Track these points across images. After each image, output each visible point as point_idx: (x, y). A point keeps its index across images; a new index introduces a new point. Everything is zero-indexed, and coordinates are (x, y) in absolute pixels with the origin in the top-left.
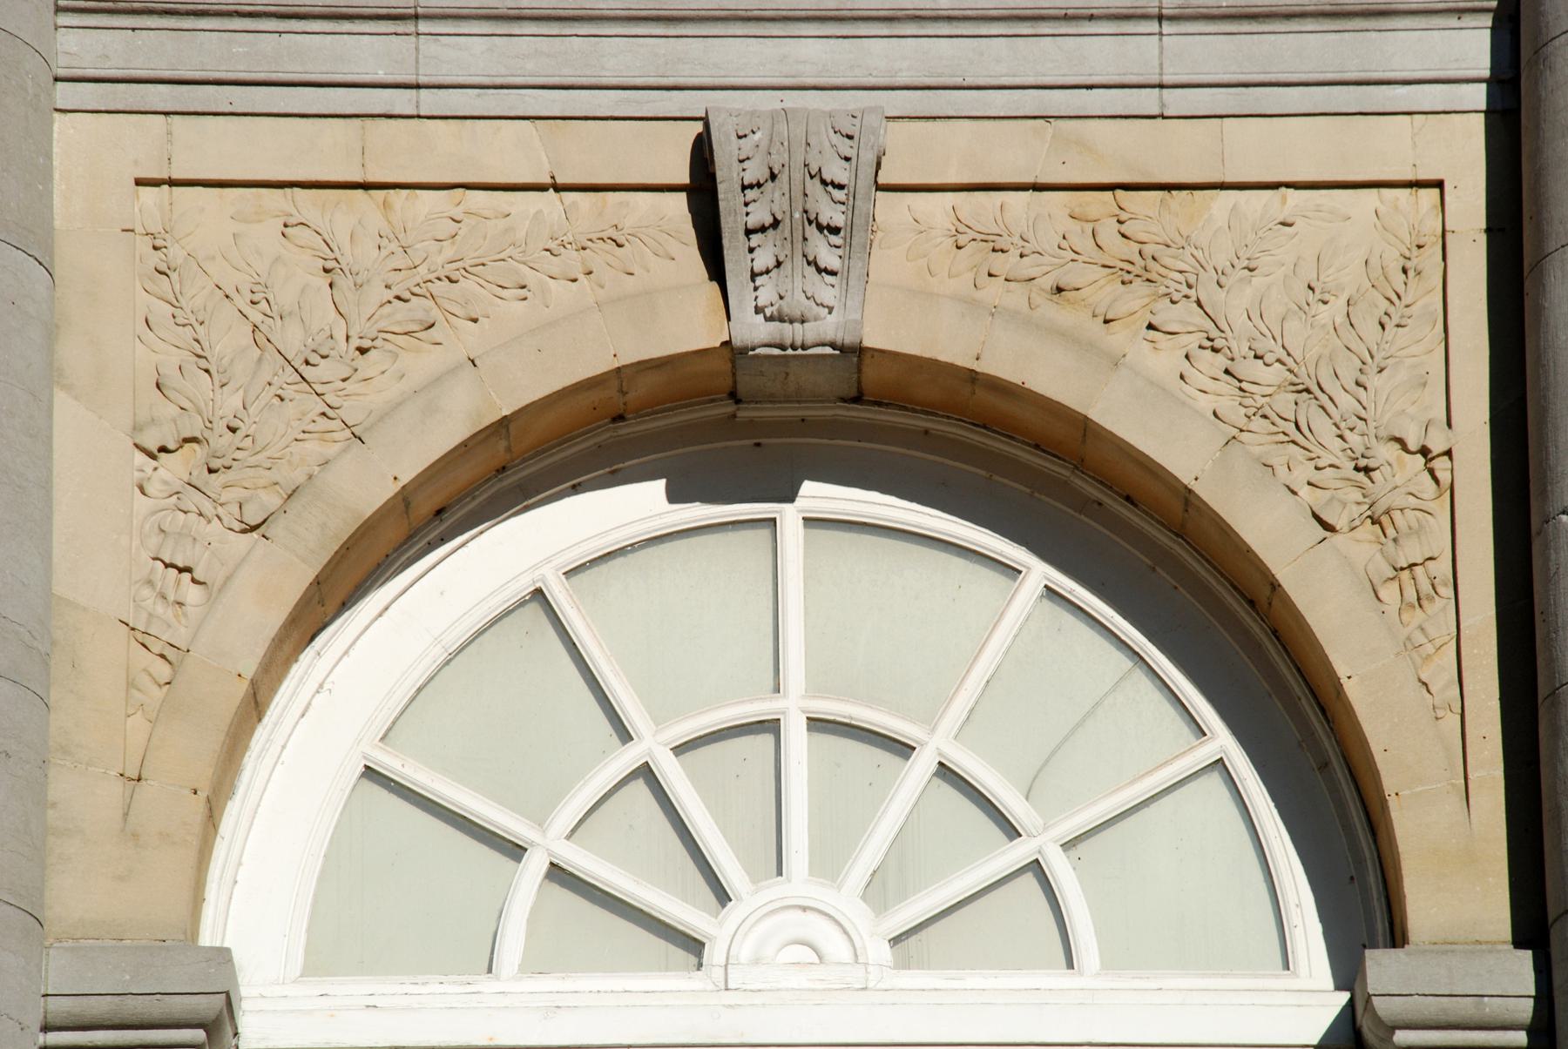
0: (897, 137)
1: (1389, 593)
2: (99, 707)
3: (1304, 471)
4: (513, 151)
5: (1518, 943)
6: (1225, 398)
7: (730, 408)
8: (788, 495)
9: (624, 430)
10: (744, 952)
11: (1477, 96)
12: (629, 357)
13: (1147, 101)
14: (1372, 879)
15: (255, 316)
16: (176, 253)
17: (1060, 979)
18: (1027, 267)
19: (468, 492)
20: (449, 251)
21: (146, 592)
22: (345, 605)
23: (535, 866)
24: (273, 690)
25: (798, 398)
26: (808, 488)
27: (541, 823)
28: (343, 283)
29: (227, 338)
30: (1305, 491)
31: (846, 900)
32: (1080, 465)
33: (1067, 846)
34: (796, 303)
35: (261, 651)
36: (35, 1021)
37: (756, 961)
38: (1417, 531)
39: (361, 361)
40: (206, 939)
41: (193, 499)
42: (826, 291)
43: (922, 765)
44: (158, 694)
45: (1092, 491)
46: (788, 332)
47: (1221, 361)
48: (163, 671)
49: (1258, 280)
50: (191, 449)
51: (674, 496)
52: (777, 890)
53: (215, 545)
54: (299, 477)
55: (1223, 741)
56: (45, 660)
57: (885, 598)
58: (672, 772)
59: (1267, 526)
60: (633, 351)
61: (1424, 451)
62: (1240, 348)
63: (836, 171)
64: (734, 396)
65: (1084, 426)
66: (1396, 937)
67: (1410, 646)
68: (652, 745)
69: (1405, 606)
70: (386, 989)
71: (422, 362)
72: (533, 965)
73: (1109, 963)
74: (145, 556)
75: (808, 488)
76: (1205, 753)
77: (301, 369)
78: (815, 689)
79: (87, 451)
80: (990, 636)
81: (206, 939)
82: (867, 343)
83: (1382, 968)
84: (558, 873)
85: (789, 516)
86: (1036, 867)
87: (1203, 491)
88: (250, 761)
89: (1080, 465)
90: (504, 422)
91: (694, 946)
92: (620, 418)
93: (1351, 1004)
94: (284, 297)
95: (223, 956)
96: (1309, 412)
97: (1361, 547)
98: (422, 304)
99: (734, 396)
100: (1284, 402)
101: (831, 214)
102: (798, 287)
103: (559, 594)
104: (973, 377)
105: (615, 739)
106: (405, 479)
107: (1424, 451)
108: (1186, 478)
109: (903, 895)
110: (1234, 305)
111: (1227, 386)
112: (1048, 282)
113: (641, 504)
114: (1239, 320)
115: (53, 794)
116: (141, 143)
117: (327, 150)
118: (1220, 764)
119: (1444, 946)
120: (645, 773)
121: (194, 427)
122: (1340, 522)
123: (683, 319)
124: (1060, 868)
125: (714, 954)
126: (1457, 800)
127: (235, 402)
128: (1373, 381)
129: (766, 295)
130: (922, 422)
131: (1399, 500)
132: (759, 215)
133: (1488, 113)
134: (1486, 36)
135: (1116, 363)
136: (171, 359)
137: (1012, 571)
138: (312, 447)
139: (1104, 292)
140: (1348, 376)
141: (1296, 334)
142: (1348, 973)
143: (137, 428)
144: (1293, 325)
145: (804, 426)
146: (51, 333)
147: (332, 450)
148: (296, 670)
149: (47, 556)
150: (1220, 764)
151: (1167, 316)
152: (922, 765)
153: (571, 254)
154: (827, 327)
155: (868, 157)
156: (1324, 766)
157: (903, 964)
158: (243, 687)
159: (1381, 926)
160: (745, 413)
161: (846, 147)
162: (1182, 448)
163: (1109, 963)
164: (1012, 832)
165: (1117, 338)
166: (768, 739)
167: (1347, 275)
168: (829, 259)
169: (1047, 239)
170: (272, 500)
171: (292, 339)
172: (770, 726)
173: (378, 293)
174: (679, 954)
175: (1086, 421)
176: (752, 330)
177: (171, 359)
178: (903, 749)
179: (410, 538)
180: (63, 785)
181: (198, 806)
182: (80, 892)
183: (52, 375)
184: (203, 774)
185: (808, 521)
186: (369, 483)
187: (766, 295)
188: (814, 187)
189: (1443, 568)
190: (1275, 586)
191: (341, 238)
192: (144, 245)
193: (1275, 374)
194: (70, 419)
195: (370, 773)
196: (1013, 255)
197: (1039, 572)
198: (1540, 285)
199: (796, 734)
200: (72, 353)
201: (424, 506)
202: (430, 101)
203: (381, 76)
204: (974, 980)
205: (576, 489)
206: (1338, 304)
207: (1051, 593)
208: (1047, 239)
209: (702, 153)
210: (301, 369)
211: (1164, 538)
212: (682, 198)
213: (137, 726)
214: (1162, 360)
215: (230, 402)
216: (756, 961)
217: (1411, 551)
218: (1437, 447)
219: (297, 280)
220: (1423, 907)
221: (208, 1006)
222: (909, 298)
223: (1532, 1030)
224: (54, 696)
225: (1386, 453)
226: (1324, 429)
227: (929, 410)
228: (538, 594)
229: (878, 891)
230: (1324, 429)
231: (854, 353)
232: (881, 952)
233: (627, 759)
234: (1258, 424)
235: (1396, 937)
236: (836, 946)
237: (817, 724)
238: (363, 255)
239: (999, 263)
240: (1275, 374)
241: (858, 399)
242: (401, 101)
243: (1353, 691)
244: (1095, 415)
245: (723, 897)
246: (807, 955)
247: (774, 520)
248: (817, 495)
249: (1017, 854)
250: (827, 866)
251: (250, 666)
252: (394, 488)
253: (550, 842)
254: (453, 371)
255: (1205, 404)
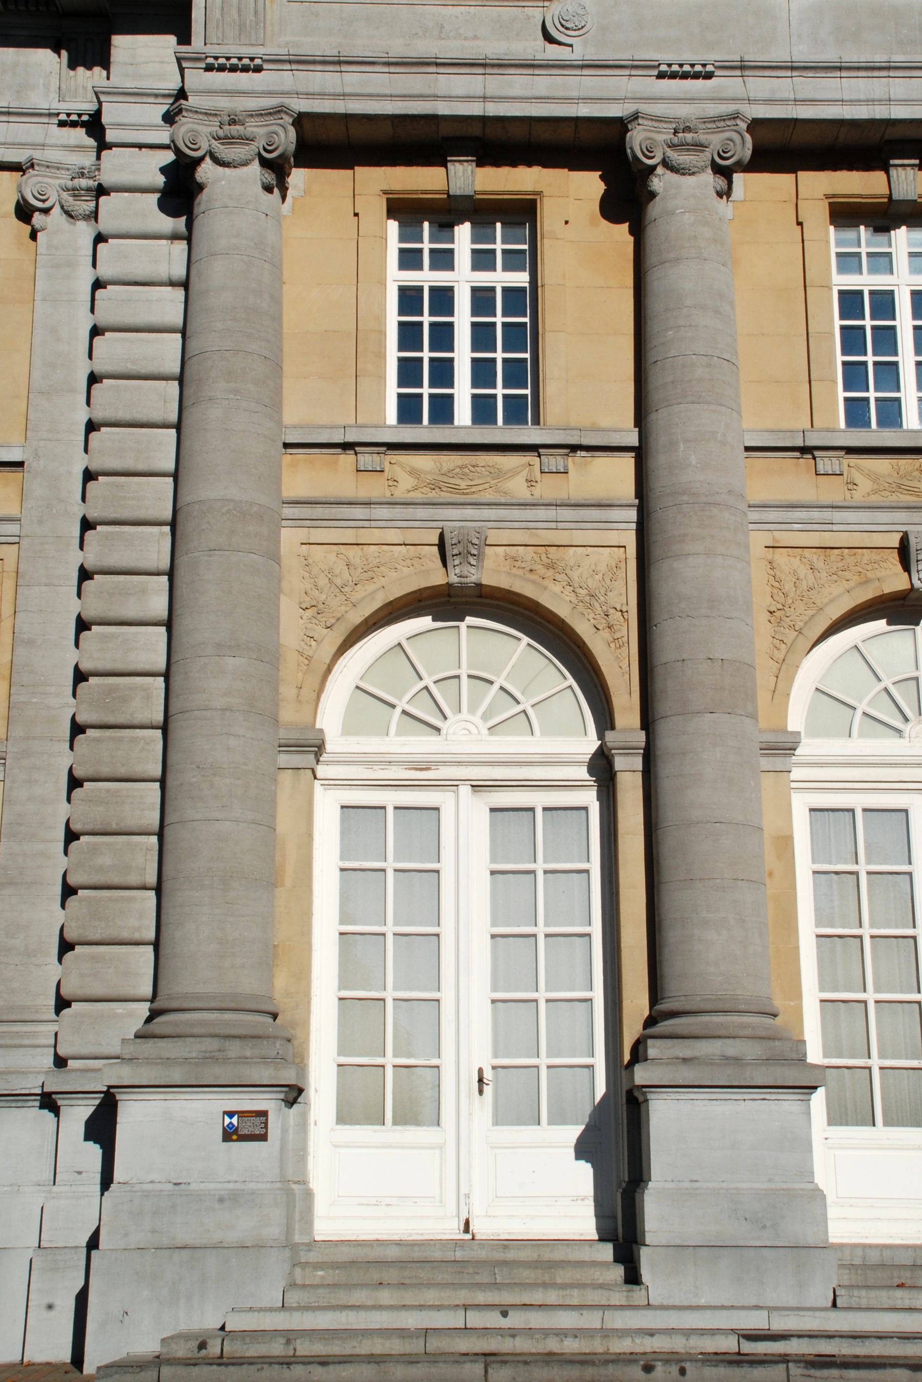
0: (490, 533)
1: (612, 645)
2: (291, 671)
3: (591, 616)
4: (393, 536)
5: (642, 729)
6: (572, 597)
7: (448, 599)
8: (463, 620)
9: (422, 604)
10: (451, 731)
11: (634, 526)
12: (423, 586)
13: (553, 525)
14: (607, 714)
15: (330, 576)
16: (310, 561)
17: (530, 738)
18: (523, 565)
19: (382, 619)
20: (378, 560)
21: (302, 643)
22: (351, 646)
23: (398, 710)
24: (333, 666)
25: (466, 596)
26: (468, 618)
27: (400, 699)
28: (352, 568)
29: (323, 582)
30: (592, 620)
31: (477, 719)
32: (537, 613)
33: (533, 706)
34: (465, 573)
35: (330, 657)
36: (276, 744)
37: (454, 734)
38: (619, 630)
39: (356, 587)
40: (318, 726)
41: (314, 620)
42: (473, 570)
43: (496, 687)
44: (305, 667)
45: (539, 620)
46: (463, 580)
47: (572, 588)
48: (306, 662)
49: (581, 569)
50: (315, 609)
51: (434, 620)
52: (460, 717)
53: (320, 631)
54: (340, 615)
55: (571, 681)
56: (278, 659)
57: (479, 642)
58: (434, 689)
59: (583, 628)
60: (424, 584)
61: (621, 611)
62: (576, 585)
63: (475, 541)
64: (449, 596)
65: (537, 604)
66: (613, 728)
67: (617, 658)
68: (428, 681)
69: (616, 648)
70: (362, 739)
71: (371, 587)
72: (398, 733)
73: (542, 734)
74: (302, 634)
75: (468, 618)
76: (567, 684)
77: (340, 589)
78: (470, 666)
79: (288, 609)
80: (515, 655)
81: (318, 726)
82: (483, 583)
83: (610, 736)
84: (404, 712)
85: (463, 625)
86: (524, 711)
87: (567, 620)
88: (328, 684)
89: (537, 613)
90: (391, 602)
91: (438, 730)
92: (420, 601)
93: (601, 745)
94: (337, 571)
95: (321, 731)
96: (593, 601)
97: (606, 634)
98: (371, 572)
99: (449, 596)
100: (587, 599)
101: (475, 552)
102: (466, 569)
103: (405, 645)
104: (509, 592)
105: (391, 709)
106: (366, 615)
107: (621, 611)
108: (563, 617)
109: (491, 718)
110: (575, 575)
111: (573, 594)
112: (528, 569)
113: (426, 622)
114: (576, 579)
115: (280, 691)
116: (302, 534)
117: (348, 536)
118: (570, 687)
119: (624, 730)
120: (426, 688)
121: (314, 603)
122: (601, 628)
123: (438, 578)
124: (531, 712)
125: (443, 732)
126: (627, 696)
127: (324, 597)
128: (609, 594)
129: (457, 571)
130: (496, 602)
131: (615, 622)
132: (456, 551)
133: (636, 530)
134: (635, 512)
135: (545, 588)
136: (309, 587)
137: (519, 639)
138: (343, 608)
139: (542, 571)
140: (603, 591)
141: (590, 582)
142: (601, 736)
143: (300, 603)
144: (589, 580)
145: (466, 603)
146: (280, 581)
147: (348, 609)
148: (339, 662)
149: (278, 634)
150: (570, 687)
151: (558, 577)
152: (496, 687)
153: (409, 562)
154: (473, 579)
155: (483, 538)
156: (596, 686)
157: (491, 734)
158: (326, 666)
159: (609, 725)
160: (452, 600)
161: (478, 535)
162: (562, 610)
163: (542, 734)
164: (518, 703)
165: (546, 582)
166: (457, 680)
167: (602, 568)
168: (473, 562)
169: (528, 558)
170: (333, 621)
171: (338, 582)
172: (458, 677)
173: (360, 570)
174: (434, 732)
175: (538, 603)
176: (454, 579)
177: (309, 587)
178: (491, 683)
179: (367, 630)
180: (283, 689)
181: (315, 694)
182: (287, 714)
183: (280, 590)
184: (317, 687)
185: (468, 627)
186: (357, 617)
187: (457, 571)
188: (470, 545)
189: (625, 639)
190: (584, 643)
191: (351, 557)
192: (302, 559)
193: (584, 592)
194: (284, 601)
195: (357, 687)
196: (520, 562)
197: (526, 640)
198: (649, 572)
199: (464, 678)
200: (285, 585)
201: (371, 622)
202: (373, 524)
203: (362, 518)
204: (509, 738)
205: (409, 618)
206: (600, 575)
207: (529, 645)
208: (528, 558)
209: (442, 536)
210: (340, 589)
211: (557, 632)
212: (436, 547)
213: (300, 675)
214: (557, 588)
215: (323, 597)
216: (454, 734)
217: (618, 635)
218: (624, 610)
219: (340, 567)
220: (619, 721)
221: (318, 742)
222: (493, 572)
223: (644, 750)
224: (280, 668)
225: (613, 611)
226: (597, 605)
227: (498, 599)
228: (399, 644)
229: (485, 717)
230: (597, 605)
231: (479, 585)
232: (486, 732)
233: (421, 685)
234: (581, 604)
235: (613, 728)
236: (474, 730)
237: (470, 676)
238: (357, 561)
239: (516, 564)
240: (584, 592)
241: (481, 596)
242: (366, 524)
243: (603, 669)
244: (540, 601)
245: (446, 718)
246: (467, 732)
247: (593, 1066)
248: (470, 620)
249: (519, 708)
250: (472, 710)
251: (328, 661)
252: (363, 618)
253: (402, 705)
254: (378, 590)
255: (568, 599)
